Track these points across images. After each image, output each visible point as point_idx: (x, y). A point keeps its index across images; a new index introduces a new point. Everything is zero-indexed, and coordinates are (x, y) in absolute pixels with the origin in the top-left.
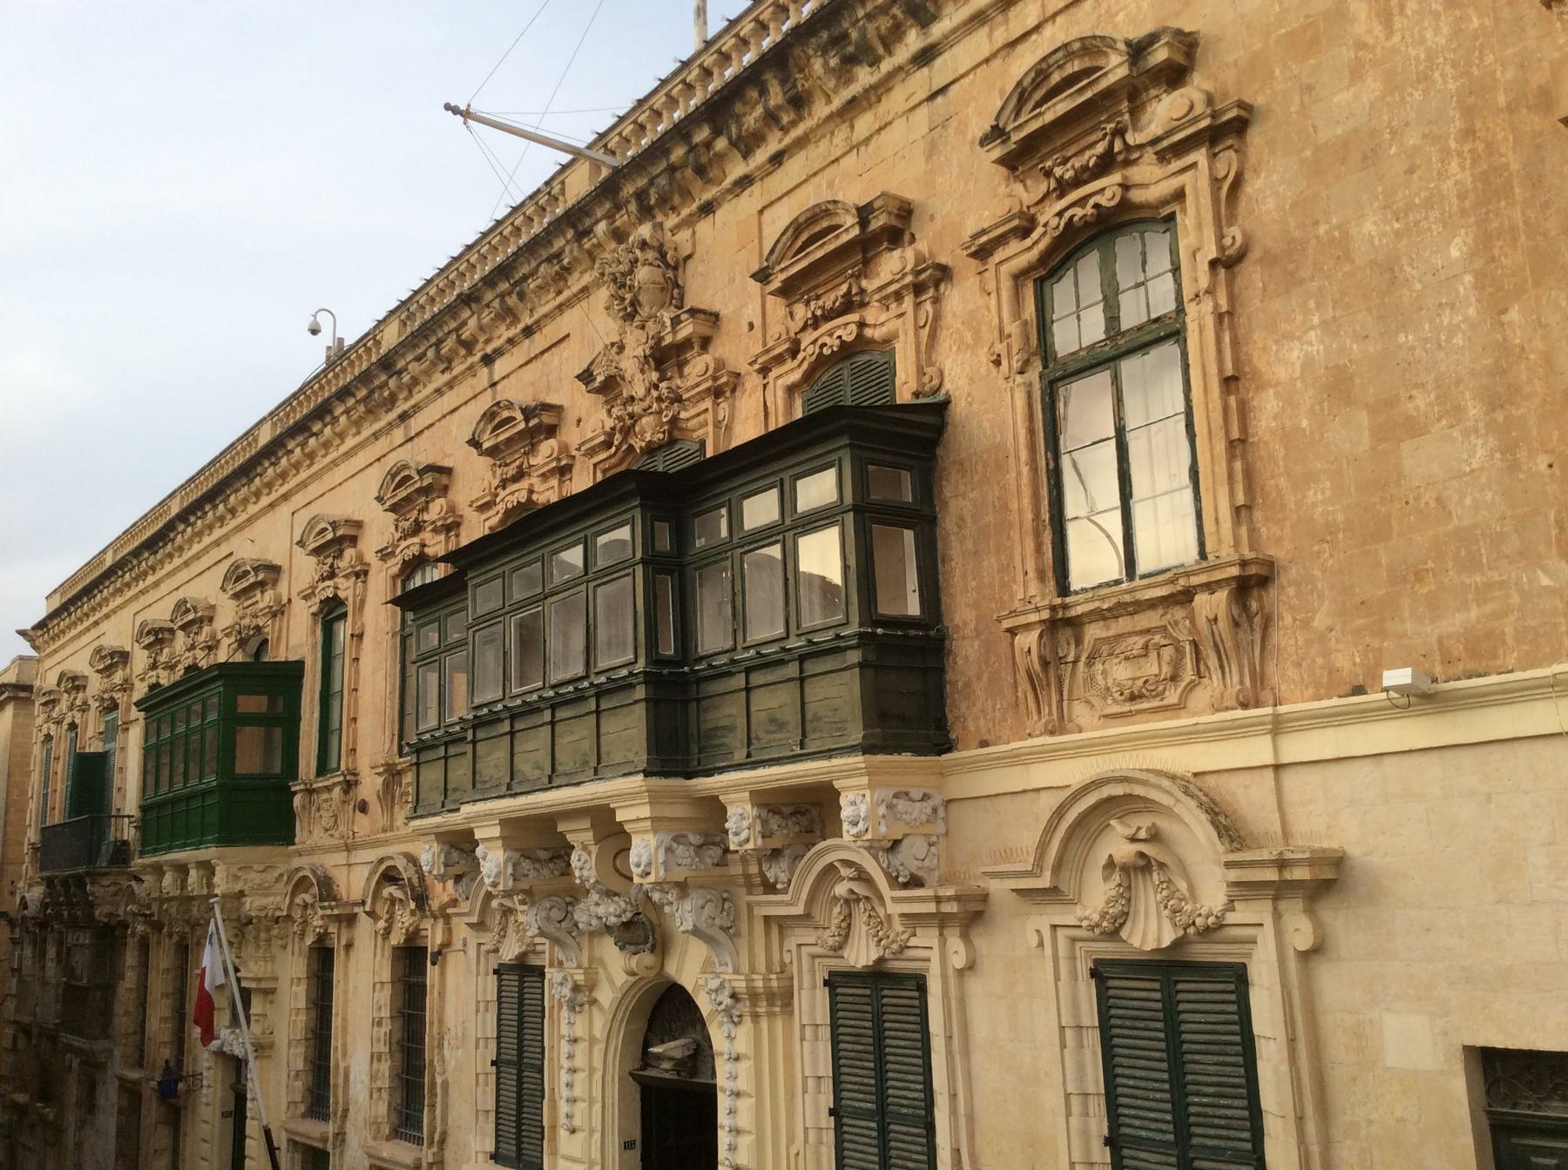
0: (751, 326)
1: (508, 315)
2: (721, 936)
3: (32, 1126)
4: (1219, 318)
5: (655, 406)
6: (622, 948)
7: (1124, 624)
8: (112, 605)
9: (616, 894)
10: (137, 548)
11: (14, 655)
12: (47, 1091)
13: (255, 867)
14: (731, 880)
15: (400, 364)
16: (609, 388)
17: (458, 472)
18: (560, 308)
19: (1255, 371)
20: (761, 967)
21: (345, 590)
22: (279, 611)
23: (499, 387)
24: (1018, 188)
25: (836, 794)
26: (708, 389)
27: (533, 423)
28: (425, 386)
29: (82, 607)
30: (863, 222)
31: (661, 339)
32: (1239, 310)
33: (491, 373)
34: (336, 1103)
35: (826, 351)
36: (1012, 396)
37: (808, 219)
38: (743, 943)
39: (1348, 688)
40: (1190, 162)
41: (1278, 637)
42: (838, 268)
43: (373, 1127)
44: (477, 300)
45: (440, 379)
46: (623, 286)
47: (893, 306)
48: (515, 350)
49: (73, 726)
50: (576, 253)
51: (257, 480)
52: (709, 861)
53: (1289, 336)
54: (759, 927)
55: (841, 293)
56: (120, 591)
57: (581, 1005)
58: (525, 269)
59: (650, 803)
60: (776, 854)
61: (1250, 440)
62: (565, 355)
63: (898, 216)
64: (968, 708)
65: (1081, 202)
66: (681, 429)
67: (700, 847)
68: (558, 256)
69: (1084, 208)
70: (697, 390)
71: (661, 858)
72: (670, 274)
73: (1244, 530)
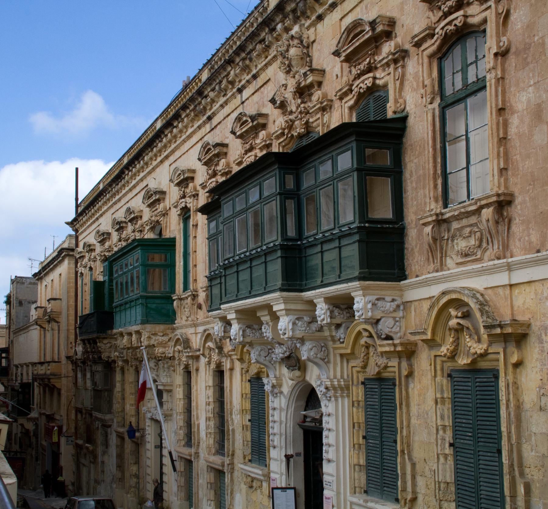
0: (337, 76)
1: (246, 69)
2: (321, 362)
3: (85, 455)
4: (498, 80)
5: (299, 116)
6: (288, 368)
7: (465, 222)
8: (103, 210)
9: (283, 344)
10: (110, 182)
11: (67, 235)
12: (90, 439)
13: (159, 334)
14: (325, 339)
15: (206, 93)
16: (282, 106)
17: (230, 146)
18: (266, 66)
19: (511, 106)
20: (339, 375)
21: (190, 203)
22: (165, 214)
23: (245, 104)
24: (431, 14)
25: (352, 299)
26: (319, 108)
27: (255, 123)
28: (217, 103)
29: (91, 211)
30: (373, 29)
31: (300, 83)
32: (507, 76)
33: (242, 97)
34: (195, 439)
35: (362, 91)
36: (427, 114)
37: (352, 27)
38: (331, 366)
39: (535, 250)
40: (488, 5)
41: (514, 228)
42: (365, 52)
43: (208, 449)
44: (233, 62)
45: (222, 100)
46: (284, 57)
47: (387, 69)
48: (250, 86)
49: (91, 269)
50: (270, 39)
51: (155, 149)
52: (314, 329)
53: (523, 89)
54: (338, 359)
55: (366, 63)
56: (105, 203)
57: (276, 394)
58: (251, 47)
59: (284, 303)
60: (338, 326)
61: (509, 137)
62: (269, 88)
63: (388, 25)
64: (412, 260)
65: (449, 23)
66: (310, 127)
67: (310, 323)
68: (263, 40)
69: (451, 25)
70: (315, 108)
71: (290, 327)
72: (305, 51)
73: (502, 180)
